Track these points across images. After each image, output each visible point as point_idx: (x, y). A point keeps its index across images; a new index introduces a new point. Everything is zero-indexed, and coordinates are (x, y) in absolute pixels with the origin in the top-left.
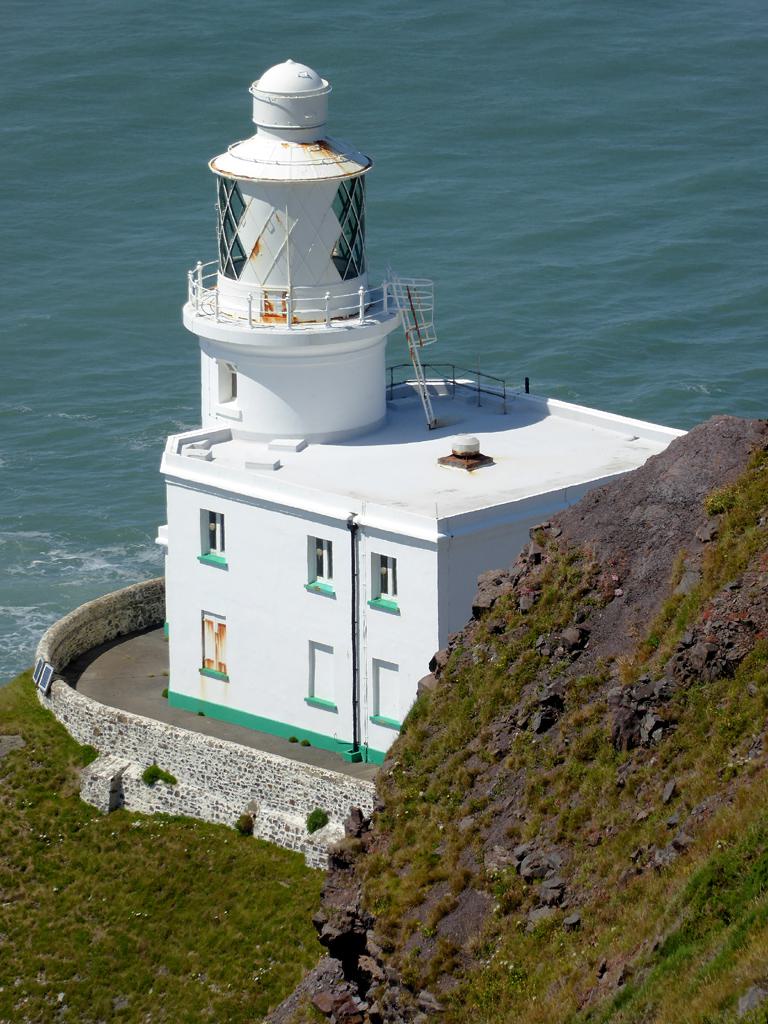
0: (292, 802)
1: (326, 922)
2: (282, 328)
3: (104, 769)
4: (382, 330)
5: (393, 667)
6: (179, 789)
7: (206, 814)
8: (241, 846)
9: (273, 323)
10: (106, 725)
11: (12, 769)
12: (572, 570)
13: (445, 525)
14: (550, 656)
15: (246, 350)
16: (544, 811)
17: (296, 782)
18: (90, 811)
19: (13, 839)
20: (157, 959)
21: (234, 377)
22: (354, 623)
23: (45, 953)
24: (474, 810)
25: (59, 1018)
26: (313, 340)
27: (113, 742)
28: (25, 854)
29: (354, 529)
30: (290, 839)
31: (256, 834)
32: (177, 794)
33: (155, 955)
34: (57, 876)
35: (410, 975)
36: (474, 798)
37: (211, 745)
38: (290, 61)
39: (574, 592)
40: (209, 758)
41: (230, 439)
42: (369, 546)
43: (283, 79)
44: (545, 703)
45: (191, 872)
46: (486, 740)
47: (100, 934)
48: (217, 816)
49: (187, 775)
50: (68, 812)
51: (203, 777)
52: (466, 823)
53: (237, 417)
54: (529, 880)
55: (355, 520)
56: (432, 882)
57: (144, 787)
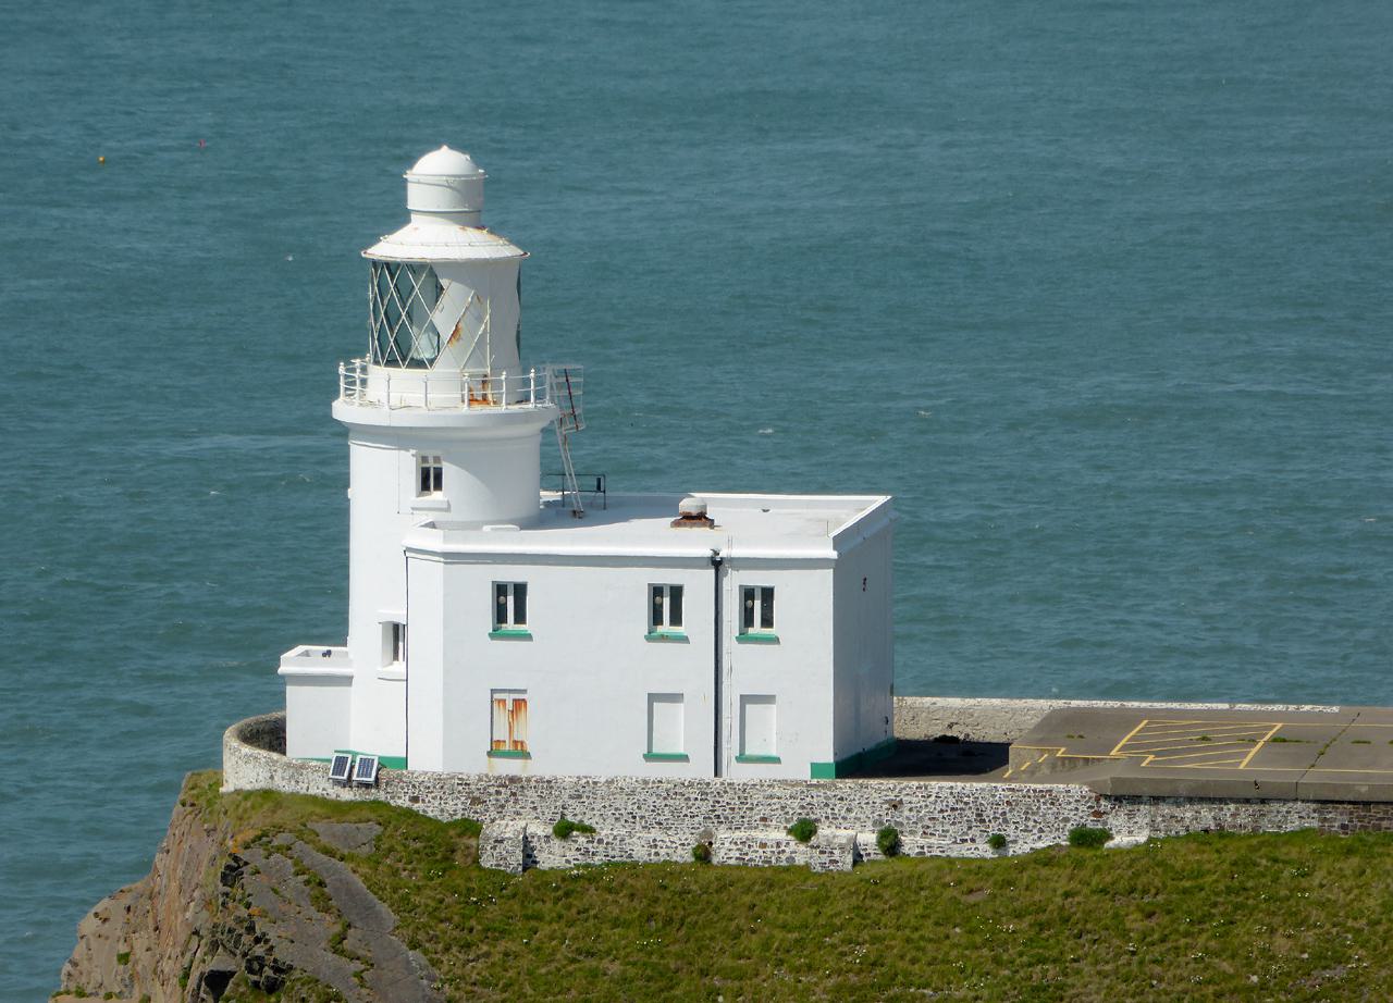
2: (478, 409)
7: (641, 853)
10: (492, 790)
17: (771, 797)
22: (492, 718)
27: (503, 806)
30: (769, 855)
31: (715, 860)
38: (445, 148)
42: (734, 582)
48: (657, 854)
51: (634, 817)
53: (445, 506)
57: (556, 843)
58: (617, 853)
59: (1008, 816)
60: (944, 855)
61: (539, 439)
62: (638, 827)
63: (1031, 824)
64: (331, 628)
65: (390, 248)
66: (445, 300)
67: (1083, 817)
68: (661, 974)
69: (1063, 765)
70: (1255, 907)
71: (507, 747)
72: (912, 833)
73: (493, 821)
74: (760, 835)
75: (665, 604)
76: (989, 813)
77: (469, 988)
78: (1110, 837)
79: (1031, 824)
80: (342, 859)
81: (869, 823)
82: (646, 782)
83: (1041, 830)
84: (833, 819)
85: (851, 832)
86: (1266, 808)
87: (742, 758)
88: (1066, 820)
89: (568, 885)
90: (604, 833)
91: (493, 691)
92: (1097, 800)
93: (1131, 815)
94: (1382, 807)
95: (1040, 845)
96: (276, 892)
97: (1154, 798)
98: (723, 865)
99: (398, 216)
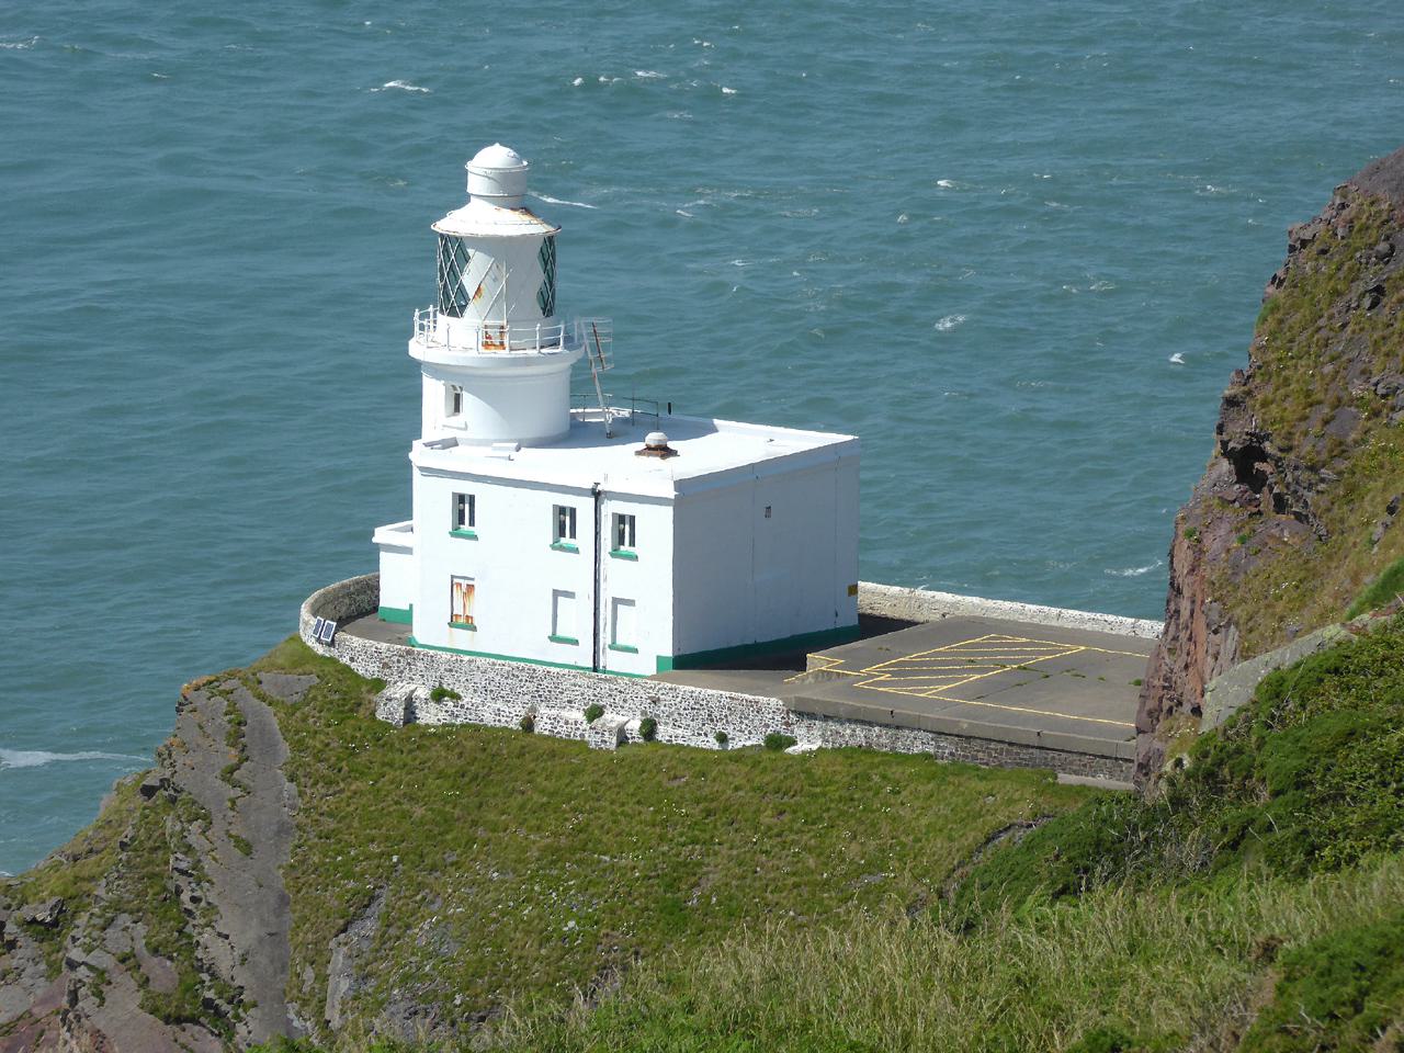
0: (570, 702)
1: (1230, 440)
3: (398, 691)
4: (573, 357)
5: (631, 603)
6: (464, 702)
7: (488, 718)
8: (528, 739)
9: (493, 350)
10: (395, 659)
11: (315, 698)
12: (1373, 209)
13: (680, 485)
14: (1367, 263)
15: (481, 372)
16: (1387, 355)
18: (386, 726)
19: (327, 749)
20: (474, 823)
21: (457, 398)
22: (596, 581)
23: (371, 829)
24: (1333, 359)
25: (398, 874)
26: (528, 361)
27: (402, 672)
28: (339, 759)
29: (597, 495)
31: (536, 731)
32: (462, 706)
33: (472, 821)
34: (371, 774)
35: (1311, 460)
36: (1330, 352)
37: (494, 664)
38: (497, 145)
39: (1378, 222)
41: (456, 445)
42: (610, 508)
43: (493, 158)
44: (1371, 291)
45: (489, 760)
46: (1331, 317)
47: (419, 811)
48: (499, 721)
49: (471, 691)
50: (368, 727)
52: (1328, 369)
53: (463, 426)
54: (1384, 396)
55: (599, 488)
56: (1311, 405)
59: (730, 719)
60: (686, 744)
61: (571, 371)
63: (744, 726)
64: (401, 509)
66: (471, 266)
67: (776, 726)
68: (446, 821)
69: (823, 676)
70: (853, 815)
71: (462, 621)
72: (666, 724)
73: (395, 683)
74: (565, 714)
75: (564, 521)
77: (317, 817)
78: (793, 742)
79: (744, 726)
80: (270, 704)
81: (638, 713)
83: (750, 733)
84: (614, 706)
86: (900, 733)
87: (613, 646)
89: (445, 733)
90: (466, 700)
91: (453, 577)
92: (788, 713)
93: (809, 728)
94: (979, 741)
95: (748, 743)
96: (201, 727)
97: (825, 716)
98: (540, 735)
99: (461, 199)
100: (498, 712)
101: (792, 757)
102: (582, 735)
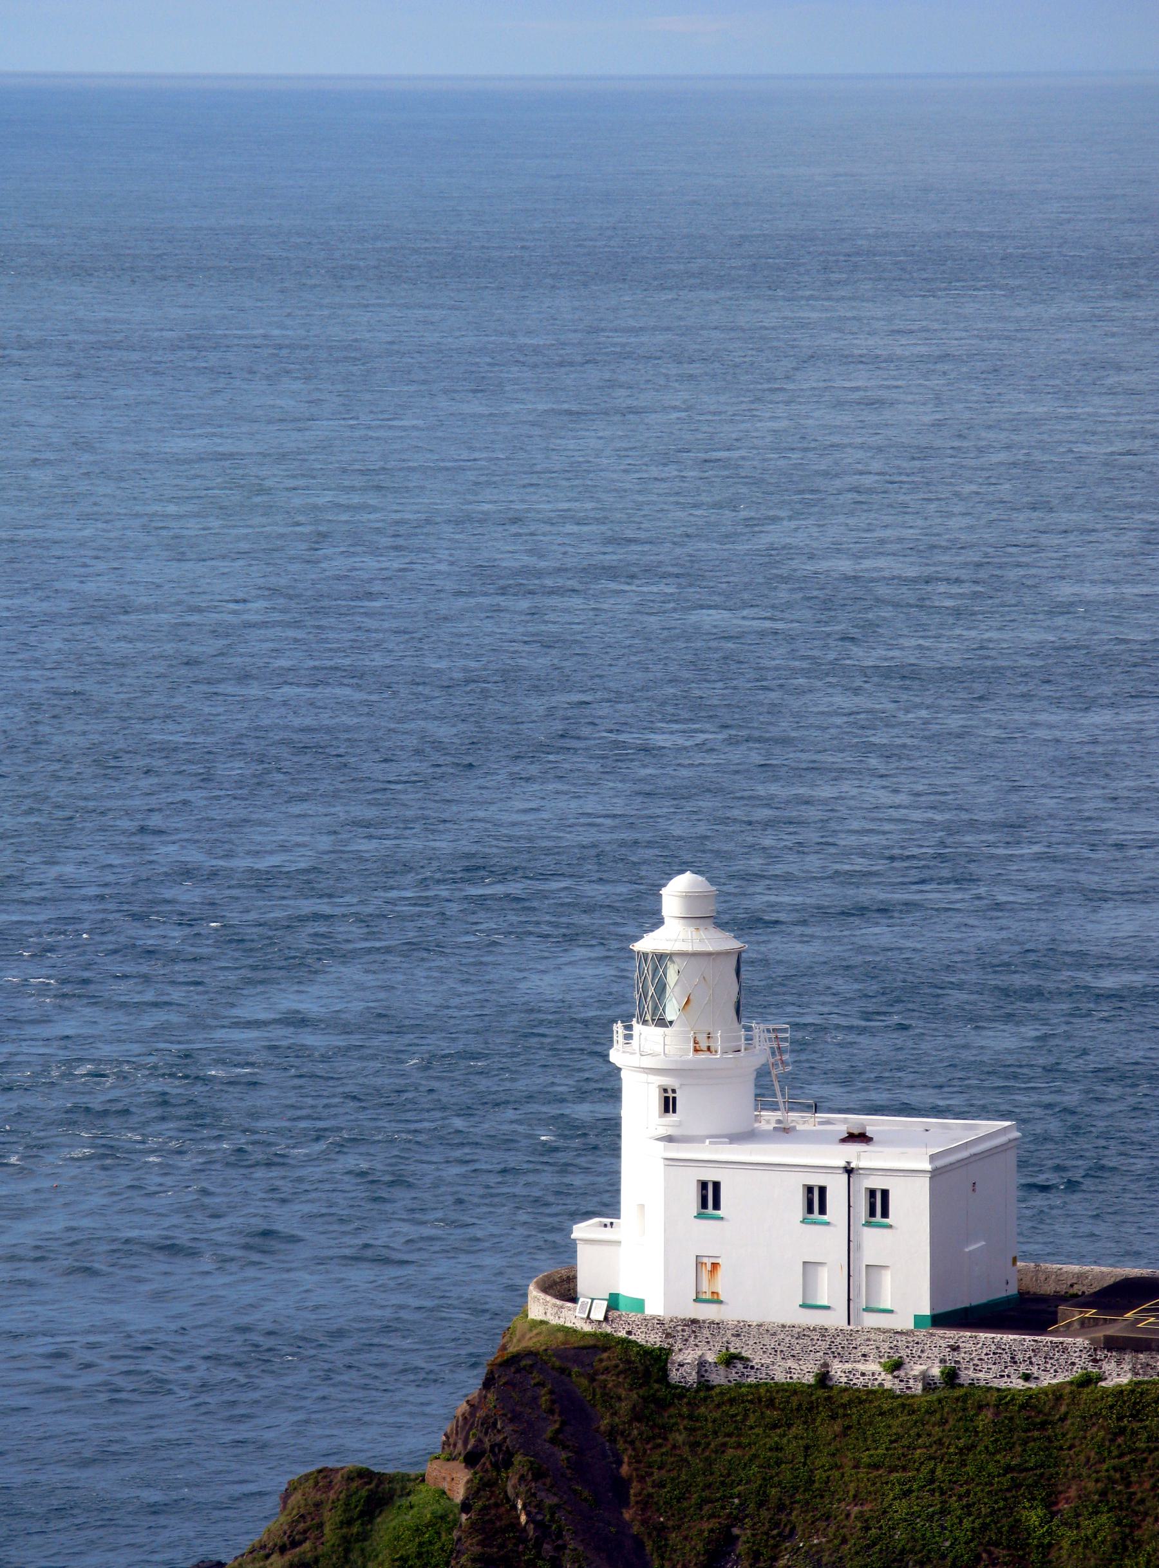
7: (780, 1377)
10: (679, 1328)
17: (869, 1340)
27: (686, 1340)
29: (849, 1171)
40: (782, 1336)
55: (852, 1165)
57: (722, 1367)
58: (763, 1376)
59: (1034, 1360)
62: (779, 1358)
63: (1049, 1366)
65: (648, 943)
71: (708, 1296)
74: (861, 1367)
76: (1019, 1357)
79: (1049, 1366)
81: (937, 1361)
82: (784, 1326)
83: (1056, 1371)
85: (924, 1367)
88: (1073, 1364)
92: (1095, 1350)
93: (1119, 1363)
95: (1054, 1381)
99: (657, 921)
100: (789, 1371)
101: (1104, 1389)
102: (881, 1385)
